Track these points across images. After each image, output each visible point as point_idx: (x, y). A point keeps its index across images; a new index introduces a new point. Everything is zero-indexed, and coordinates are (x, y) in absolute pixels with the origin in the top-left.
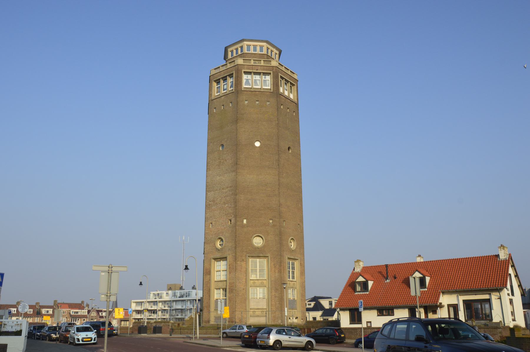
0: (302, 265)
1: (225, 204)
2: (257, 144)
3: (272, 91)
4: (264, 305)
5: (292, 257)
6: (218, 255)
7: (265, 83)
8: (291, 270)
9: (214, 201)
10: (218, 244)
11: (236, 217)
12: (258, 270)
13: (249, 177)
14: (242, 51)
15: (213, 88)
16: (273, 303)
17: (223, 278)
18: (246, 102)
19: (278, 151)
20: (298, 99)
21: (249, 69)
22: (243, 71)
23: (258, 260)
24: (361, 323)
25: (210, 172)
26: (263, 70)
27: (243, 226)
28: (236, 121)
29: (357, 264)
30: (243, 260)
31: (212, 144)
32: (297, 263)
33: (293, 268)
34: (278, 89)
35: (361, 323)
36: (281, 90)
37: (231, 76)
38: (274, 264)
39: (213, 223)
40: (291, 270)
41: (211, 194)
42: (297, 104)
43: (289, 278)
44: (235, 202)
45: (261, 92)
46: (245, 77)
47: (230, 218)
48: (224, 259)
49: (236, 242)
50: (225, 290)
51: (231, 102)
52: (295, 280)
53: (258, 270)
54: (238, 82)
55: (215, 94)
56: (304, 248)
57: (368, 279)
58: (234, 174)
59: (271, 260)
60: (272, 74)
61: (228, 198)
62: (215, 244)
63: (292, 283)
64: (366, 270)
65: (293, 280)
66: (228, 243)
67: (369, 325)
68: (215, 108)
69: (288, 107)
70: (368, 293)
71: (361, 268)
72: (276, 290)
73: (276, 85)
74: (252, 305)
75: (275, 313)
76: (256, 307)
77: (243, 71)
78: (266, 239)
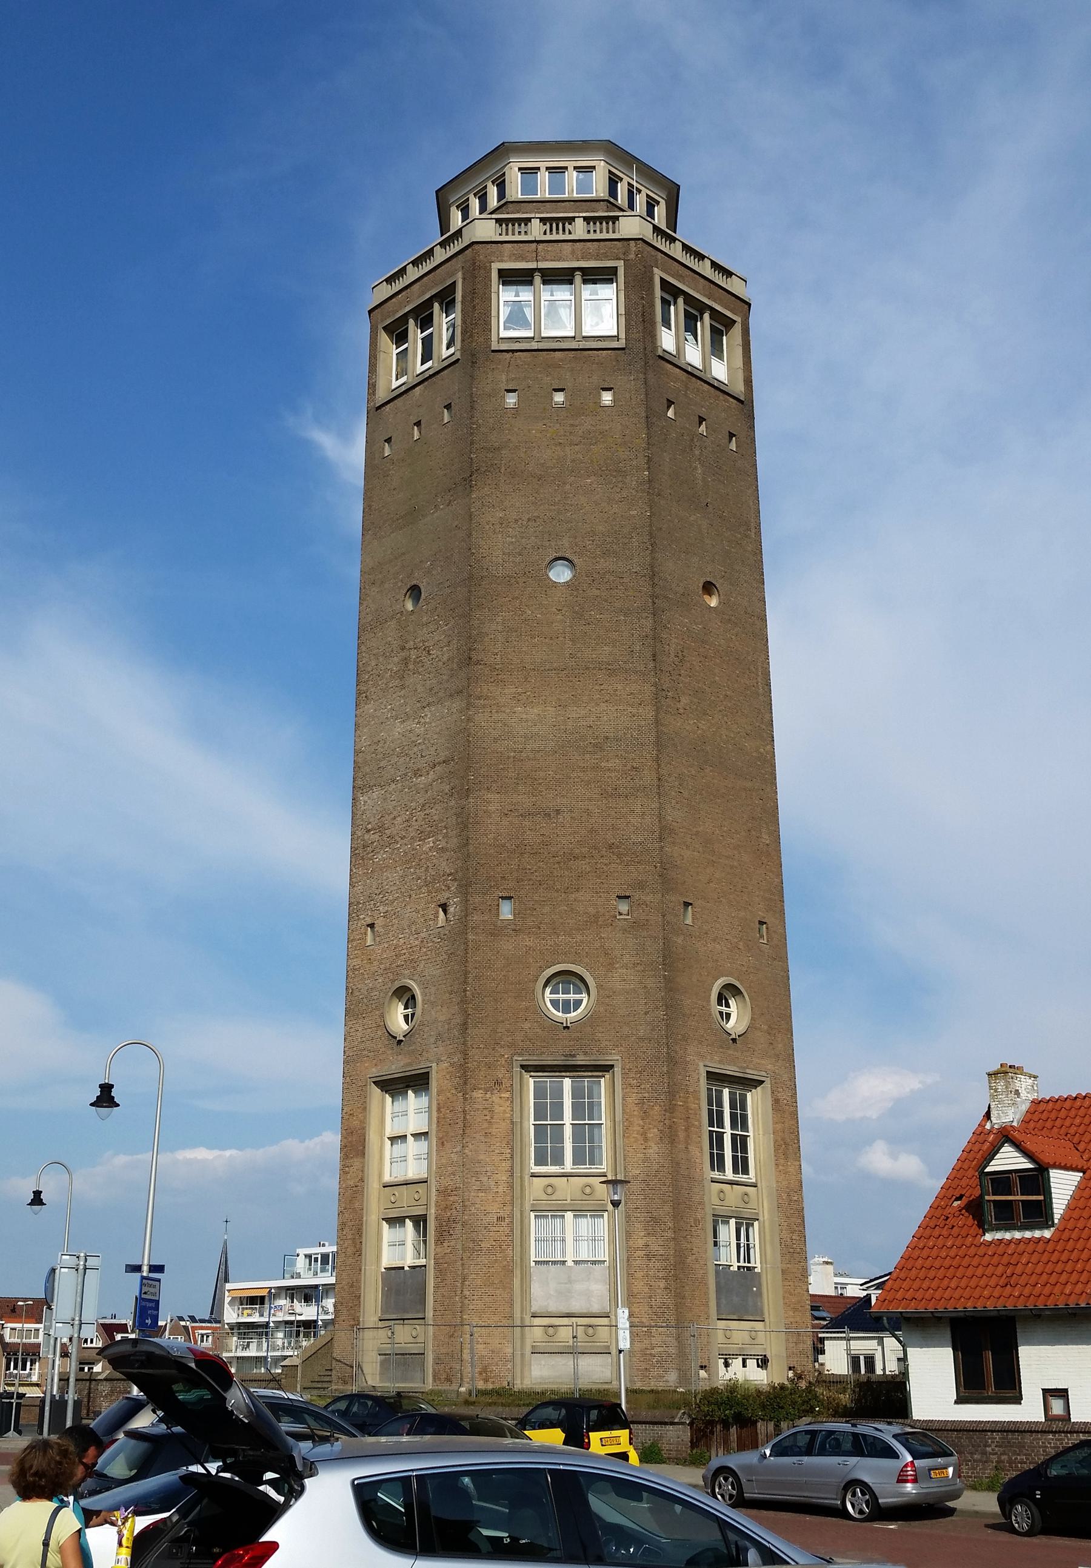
0: (786, 1111)
1: (422, 836)
2: (561, 574)
3: (622, 343)
4: (593, 1292)
5: (730, 1070)
6: (396, 1066)
7: (600, 313)
8: (728, 1131)
9: (381, 828)
10: (397, 1019)
11: (465, 888)
12: (568, 1131)
13: (524, 717)
14: (501, 195)
15: (381, 357)
16: (640, 1286)
17: (415, 1169)
18: (511, 400)
19: (654, 596)
20: (748, 382)
21: (522, 258)
22: (496, 266)
23: (567, 1083)
24: (1017, 1399)
25: (369, 708)
26: (583, 258)
27: (497, 931)
28: (467, 478)
29: (1001, 1085)
30: (498, 1083)
31: (375, 589)
32: (755, 1100)
33: (740, 1120)
34: (652, 336)
35: (1017, 1399)
36: (667, 340)
37: (446, 298)
38: (641, 1102)
39: (379, 923)
40: (728, 1131)
41: (371, 800)
42: (745, 405)
43: (721, 1168)
44: (465, 823)
45: (581, 352)
46: (506, 296)
47: (443, 897)
48: (418, 1082)
49: (464, 1001)
50: (420, 1221)
51: (448, 407)
52: (752, 1177)
53: (568, 1131)
54: (478, 319)
55: (392, 381)
56: (790, 1031)
57: (1046, 1158)
58: (457, 704)
59: (626, 1085)
60: (621, 272)
61: (435, 812)
62: (382, 1016)
63: (733, 1195)
64: (1045, 1113)
65: (582, 1169)
66: (439, 1016)
67: (1057, 1407)
68: (388, 440)
69: (703, 412)
70: (1047, 1234)
71: (1025, 1107)
72: (653, 1223)
73: (639, 319)
74: (543, 1292)
75: (649, 1334)
76: (553, 1307)
77: (496, 266)
78: (599, 987)
